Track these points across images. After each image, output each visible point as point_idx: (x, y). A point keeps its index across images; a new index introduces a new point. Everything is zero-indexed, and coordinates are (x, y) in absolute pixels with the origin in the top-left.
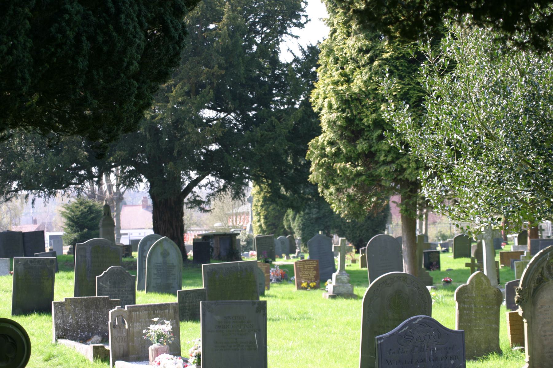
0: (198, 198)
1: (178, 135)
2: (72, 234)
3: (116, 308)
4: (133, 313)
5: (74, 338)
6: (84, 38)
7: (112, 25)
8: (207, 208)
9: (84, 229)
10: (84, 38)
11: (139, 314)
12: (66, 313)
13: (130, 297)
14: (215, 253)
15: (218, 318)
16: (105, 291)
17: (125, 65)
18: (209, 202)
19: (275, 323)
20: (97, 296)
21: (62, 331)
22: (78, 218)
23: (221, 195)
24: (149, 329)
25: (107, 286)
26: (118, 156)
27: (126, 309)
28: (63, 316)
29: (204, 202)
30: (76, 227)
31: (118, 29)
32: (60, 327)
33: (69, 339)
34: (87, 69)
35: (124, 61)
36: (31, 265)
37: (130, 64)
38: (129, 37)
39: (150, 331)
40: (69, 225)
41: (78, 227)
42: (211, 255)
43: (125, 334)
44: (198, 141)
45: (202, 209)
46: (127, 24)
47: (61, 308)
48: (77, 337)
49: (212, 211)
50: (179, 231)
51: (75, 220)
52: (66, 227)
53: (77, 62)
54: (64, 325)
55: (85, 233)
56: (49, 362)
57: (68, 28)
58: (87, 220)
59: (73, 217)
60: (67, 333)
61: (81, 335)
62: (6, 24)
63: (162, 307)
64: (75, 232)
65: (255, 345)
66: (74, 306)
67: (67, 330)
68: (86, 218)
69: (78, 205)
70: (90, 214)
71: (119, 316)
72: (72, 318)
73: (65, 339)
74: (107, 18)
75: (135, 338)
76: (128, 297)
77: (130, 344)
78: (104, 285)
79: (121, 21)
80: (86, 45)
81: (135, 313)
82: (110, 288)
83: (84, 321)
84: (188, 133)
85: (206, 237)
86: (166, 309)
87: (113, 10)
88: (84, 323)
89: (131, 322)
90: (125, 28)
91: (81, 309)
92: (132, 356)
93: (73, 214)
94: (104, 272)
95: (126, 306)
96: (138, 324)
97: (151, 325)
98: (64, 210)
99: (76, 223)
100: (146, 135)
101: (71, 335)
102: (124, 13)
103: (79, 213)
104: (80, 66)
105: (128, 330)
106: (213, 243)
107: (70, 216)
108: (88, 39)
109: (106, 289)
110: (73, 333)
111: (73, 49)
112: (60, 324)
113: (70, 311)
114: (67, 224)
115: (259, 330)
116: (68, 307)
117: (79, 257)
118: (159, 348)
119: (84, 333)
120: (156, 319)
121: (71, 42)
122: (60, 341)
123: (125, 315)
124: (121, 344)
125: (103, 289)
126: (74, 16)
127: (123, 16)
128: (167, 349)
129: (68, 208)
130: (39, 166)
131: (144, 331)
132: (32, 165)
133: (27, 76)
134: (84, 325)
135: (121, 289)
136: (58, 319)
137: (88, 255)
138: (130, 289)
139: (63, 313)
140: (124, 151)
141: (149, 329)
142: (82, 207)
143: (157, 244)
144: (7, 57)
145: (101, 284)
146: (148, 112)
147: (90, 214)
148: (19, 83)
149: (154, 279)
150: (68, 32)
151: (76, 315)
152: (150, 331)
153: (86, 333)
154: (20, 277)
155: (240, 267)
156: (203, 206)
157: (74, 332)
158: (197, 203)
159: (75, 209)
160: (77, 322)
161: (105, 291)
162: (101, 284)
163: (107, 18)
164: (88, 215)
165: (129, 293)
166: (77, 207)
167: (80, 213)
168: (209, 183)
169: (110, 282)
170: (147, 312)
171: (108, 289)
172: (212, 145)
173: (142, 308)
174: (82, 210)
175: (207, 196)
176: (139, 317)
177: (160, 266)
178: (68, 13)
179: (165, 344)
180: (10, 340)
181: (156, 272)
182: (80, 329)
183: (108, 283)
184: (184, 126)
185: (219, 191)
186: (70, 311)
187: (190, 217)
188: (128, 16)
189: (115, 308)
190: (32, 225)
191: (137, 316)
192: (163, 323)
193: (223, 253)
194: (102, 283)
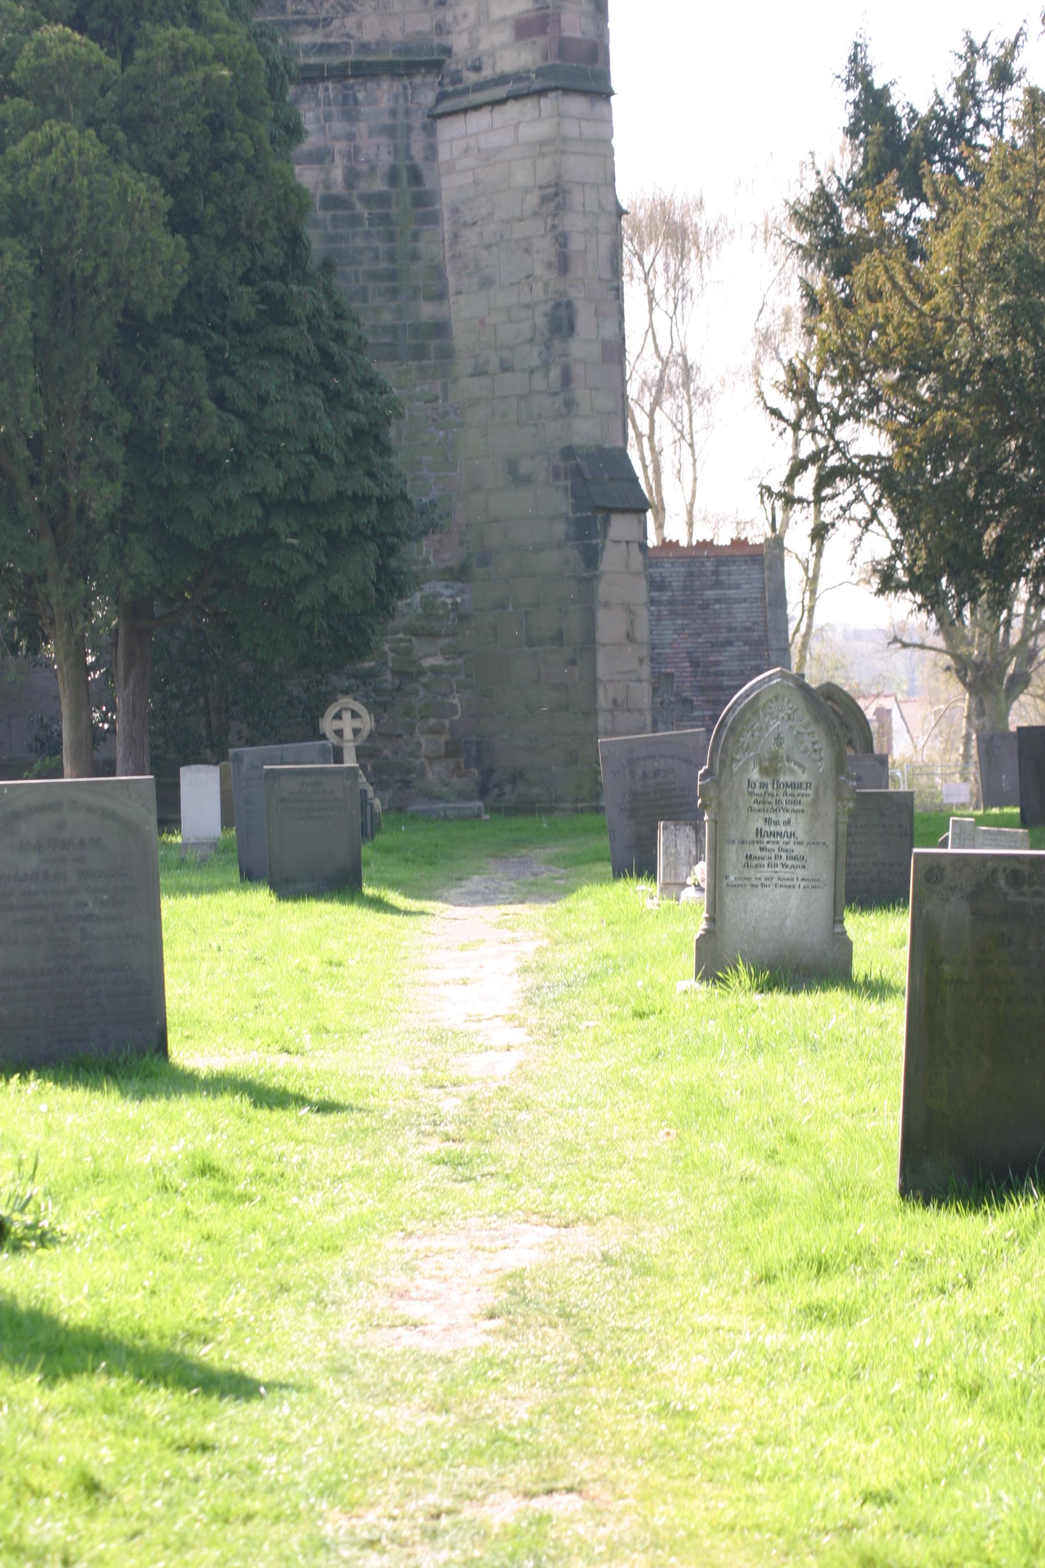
36: (1013, 897)
154: (947, 969)
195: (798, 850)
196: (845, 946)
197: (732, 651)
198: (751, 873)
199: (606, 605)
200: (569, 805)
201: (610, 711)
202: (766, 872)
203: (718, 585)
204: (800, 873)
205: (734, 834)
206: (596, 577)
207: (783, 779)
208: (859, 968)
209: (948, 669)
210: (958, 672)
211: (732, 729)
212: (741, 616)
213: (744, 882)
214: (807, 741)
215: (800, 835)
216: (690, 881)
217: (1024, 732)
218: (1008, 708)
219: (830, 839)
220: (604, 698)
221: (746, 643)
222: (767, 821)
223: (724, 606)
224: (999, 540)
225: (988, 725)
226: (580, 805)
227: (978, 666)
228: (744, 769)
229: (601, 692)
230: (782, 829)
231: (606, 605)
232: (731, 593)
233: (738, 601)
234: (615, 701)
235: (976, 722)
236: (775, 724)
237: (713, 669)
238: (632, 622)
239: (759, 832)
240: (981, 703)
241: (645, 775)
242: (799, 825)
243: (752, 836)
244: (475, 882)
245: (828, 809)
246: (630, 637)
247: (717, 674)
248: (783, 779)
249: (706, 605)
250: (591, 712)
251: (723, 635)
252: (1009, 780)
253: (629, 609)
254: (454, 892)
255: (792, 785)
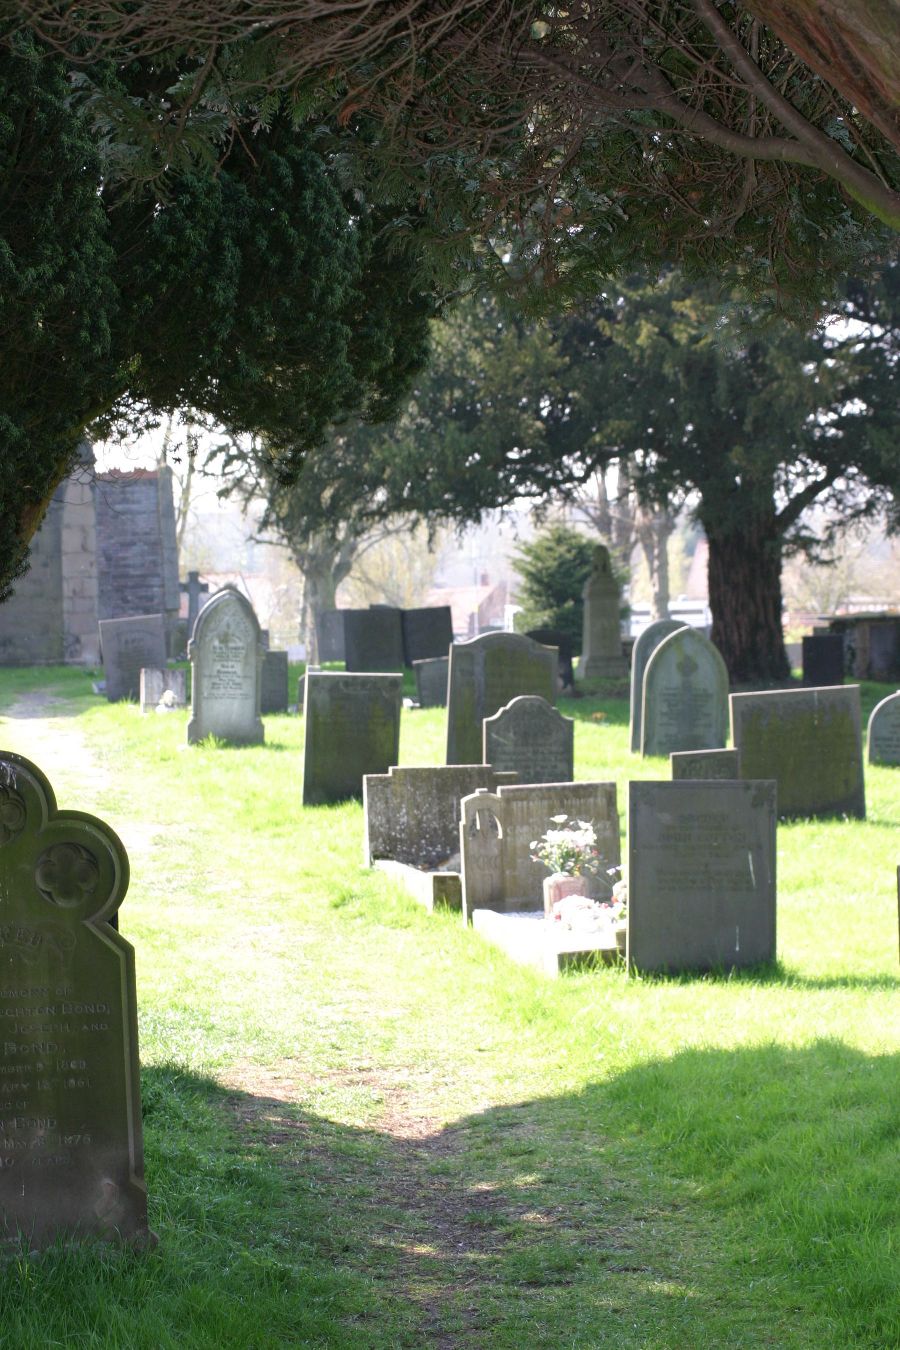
0: (804, 533)
1: (759, 380)
2: (538, 614)
3: (477, 793)
4: (515, 804)
5: (411, 858)
6: (228, 242)
7: (288, 212)
8: (825, 555)
9: (565, 600)
10: (228, 242)
11: (528, 808)
12: (395, 802)
13: (562, 767)
14: (859, 664)
15: (666, 818)
16: (505, 753)
17: (316, 294)
18: (830, 540)
19: (889, 831)
20: (485, 765)
21: (384, 842)
22: (552, 576)
23: (861, 526)
24: (545, 841)
25: (509, 741)
26: (613, 431)
27: (499, 795)
28: (388, 808)
29: (818, 542)
30: (548, 597)
31: (301, 221)
32: (381, 833)
33: (398, 861)
34: (236, 305)
35: (313, 287)
36: (345, 691)
37: (328, 291)
38: (323, 238)
39: (547, 845)
40: (532, 593)
41: (554, 596)
42: (850, 669)
43: (496, 851)
44: (801, 396)
45: (813, 560)
46: (316, 208)
47: (383, 792)
48: (418, 855)
49: (837, 563)
50: (771, 608)
51: (546, 580)
52: (525, 596)
53: (213, 290)
54: (390, 829)
55: (569, 610)
56: (341, 909)
57: (189, 223)
58: (573, 580)
59: (540, 571)
60: (396, 847)
61: (429, 852)
62: (48, 222)
63: (582, 792)
64: (545, 609)
65: (749, 881)
66: (413, 785)
67: (395, 839)
68: (572, 576)
69: (552, 545)
70: (580, 565)
71: (483, 808)
72: (407, 814)
73: (392, 859)
74: (278, 198)
75: (520, 861)
76: (556, 767)
77: (508, 873)
78: (502, 740)
79: (305, 203)
80: (232, 257)
81: (520, 804)
82: (516, 745)
83: (435, 820)
84: (778, 378)
85: (841, 625)
86: (590, 796)
87: (290, 181)
88: (435, 825)
89: (511, 824)
90: (313, 218)
91: (429, 793)
92: (510, 901)
93: (540, 565)
94: (502, 710)
95: (499, 789)
96: (526, 829)
97: (550, 832)
98: (519, 555)
99: (548, 587)
100: (678, 382)
101: (404, 852)
102: (312, 186)
103: (553, 564)
104: (220, 298)
105: (503, 843)
106: (854, 639)
107: (533, 570)
108: (237, 242)
109: (507, 749)
110: (410, 847)
111: (205, 265)
112: (381, 826)
113: (403, 797)
114: (526, 590)
115: (760, 847)
116: (399, 789)
117: (458, 674)
118: (564, 883)
119: (434, 846)
120: (560, 819)
121: (199, 249)
122: (379, 863)
123: (497, 808)
124: (487, 872)
125: (500, 749)
126: (203, 197)
127: (309, 194)
128: (584, 885)
129: (529, 551)
130: (426, 456)
131: (533, 845)
132: (410, 455)
133: (104, 324)
134: (435, 830)
135: (541, 749)
136: (377, 814)
137: (478, 670)
138: (562, 749)
139: (387, 803)
140: (628, 418)
141: (545, 841)
142: (562, 549)
143: (669, 644)
144: (54, 288)
145: (495, 736)
146: (682, 327)
147: (580, 565)
148: (86, 338)
149: (662, 725)
150: (188, 232)
151: (418, 808)
152: (547, 845)
153: (439, 848)
154: (321, 720)
155: (820, 701)
156: (816, 550)
157: (412, 844)
158: (806, 544)
159: (544, 554)
160: (420, 823)
161: (505, 753)
162: (495, 736)
163: (278, 198)
164: (575, 568)
165: (559, 757)
166: (550, 549)
167: (556, 564)
168: (834, 496)
169: (515, 733)
170: (546, 803)
171: (510, 748)
172: (853, 403)
173: (534, 794)
174: (561, 556)
175: (828, 528)
176: (528, 814)
177: (675, 695)
178: (188, 193)
179: (577, 873)
180: (85, 855)
181: (665, 710)
182: (425, 838)
183: (512, 735)
184: (768, 362)
185: (857, 514)
186: (403, 797)
187: (846, 572)
188: (321, 192)
189: (473, 792)
190: (479, 587)
191: (523, 812)
192: (576, 828)
193: (879, 664)
194: (498, 734)
195: (238, 681)
196: (261, 728)
197: (135, 550)
198: (215, 692)
199: (69, 527)
200: (43, 662)
201: (71, 598)
202: (222, 691)
203: (125, 501)
204: (239, 692)
205: (207, 672)
206: (62, 509)
207: (232, 645)
208: (268, 739)
209: (290, 559)
210: (298, 562)
211: (206, 621)
212: (142, 524)
213: (212, 696)
214: (242, 626)
215: (239, 673)
216: (161, 702)
217: (349, 615)
218: (335, 588)
219: (254, 675)
220: (67, 589)
221: (146, 544)
222: (223, 666)
223: (129, 517)
224: (333, 498)
225: (320, 602)
226: (51, 661)
227: (313, 558)
228: (212, 640)
229: (65, 586)
230: (230, 670)
231: (69, 527)
232: (135, 507)
233: (140, 513)
234: (74, 592)
235: (311, 600)
236: (227, 619)
237: (122, 563)
238: (85, 538)
239: (219, 672)
240: (315, 585)
241: (127, 642)
242: (238, 668)
243: (215, 673)
244: (17, 707)
245: (253, 660)
246: (84, 549)
247: (126, 566)
248: (232, 645)
249: (118, 514)
250: (58, 598)
251: (129, 538)
252: (338, 643)
253: (83, 530)
254: (9, 712)
255: (236, 649)
